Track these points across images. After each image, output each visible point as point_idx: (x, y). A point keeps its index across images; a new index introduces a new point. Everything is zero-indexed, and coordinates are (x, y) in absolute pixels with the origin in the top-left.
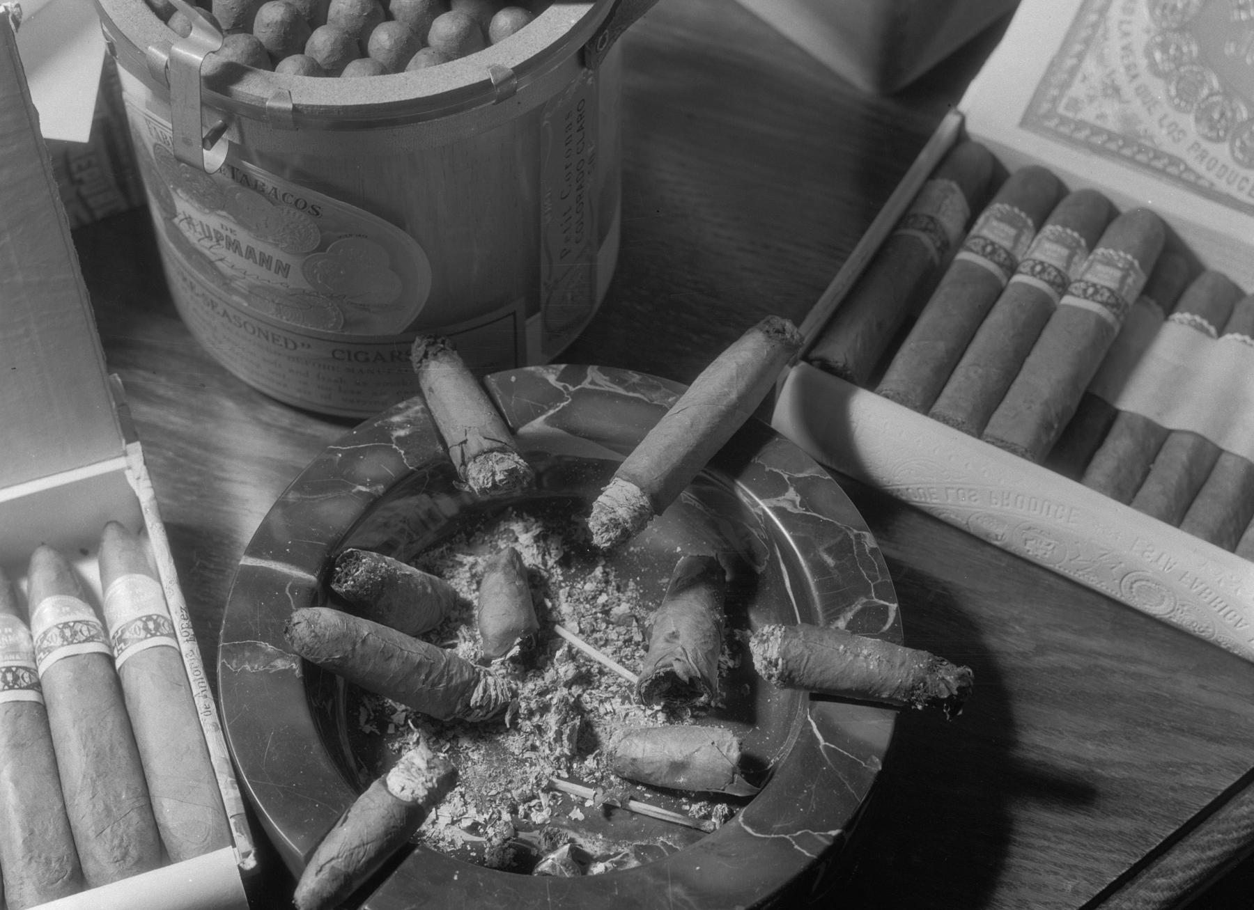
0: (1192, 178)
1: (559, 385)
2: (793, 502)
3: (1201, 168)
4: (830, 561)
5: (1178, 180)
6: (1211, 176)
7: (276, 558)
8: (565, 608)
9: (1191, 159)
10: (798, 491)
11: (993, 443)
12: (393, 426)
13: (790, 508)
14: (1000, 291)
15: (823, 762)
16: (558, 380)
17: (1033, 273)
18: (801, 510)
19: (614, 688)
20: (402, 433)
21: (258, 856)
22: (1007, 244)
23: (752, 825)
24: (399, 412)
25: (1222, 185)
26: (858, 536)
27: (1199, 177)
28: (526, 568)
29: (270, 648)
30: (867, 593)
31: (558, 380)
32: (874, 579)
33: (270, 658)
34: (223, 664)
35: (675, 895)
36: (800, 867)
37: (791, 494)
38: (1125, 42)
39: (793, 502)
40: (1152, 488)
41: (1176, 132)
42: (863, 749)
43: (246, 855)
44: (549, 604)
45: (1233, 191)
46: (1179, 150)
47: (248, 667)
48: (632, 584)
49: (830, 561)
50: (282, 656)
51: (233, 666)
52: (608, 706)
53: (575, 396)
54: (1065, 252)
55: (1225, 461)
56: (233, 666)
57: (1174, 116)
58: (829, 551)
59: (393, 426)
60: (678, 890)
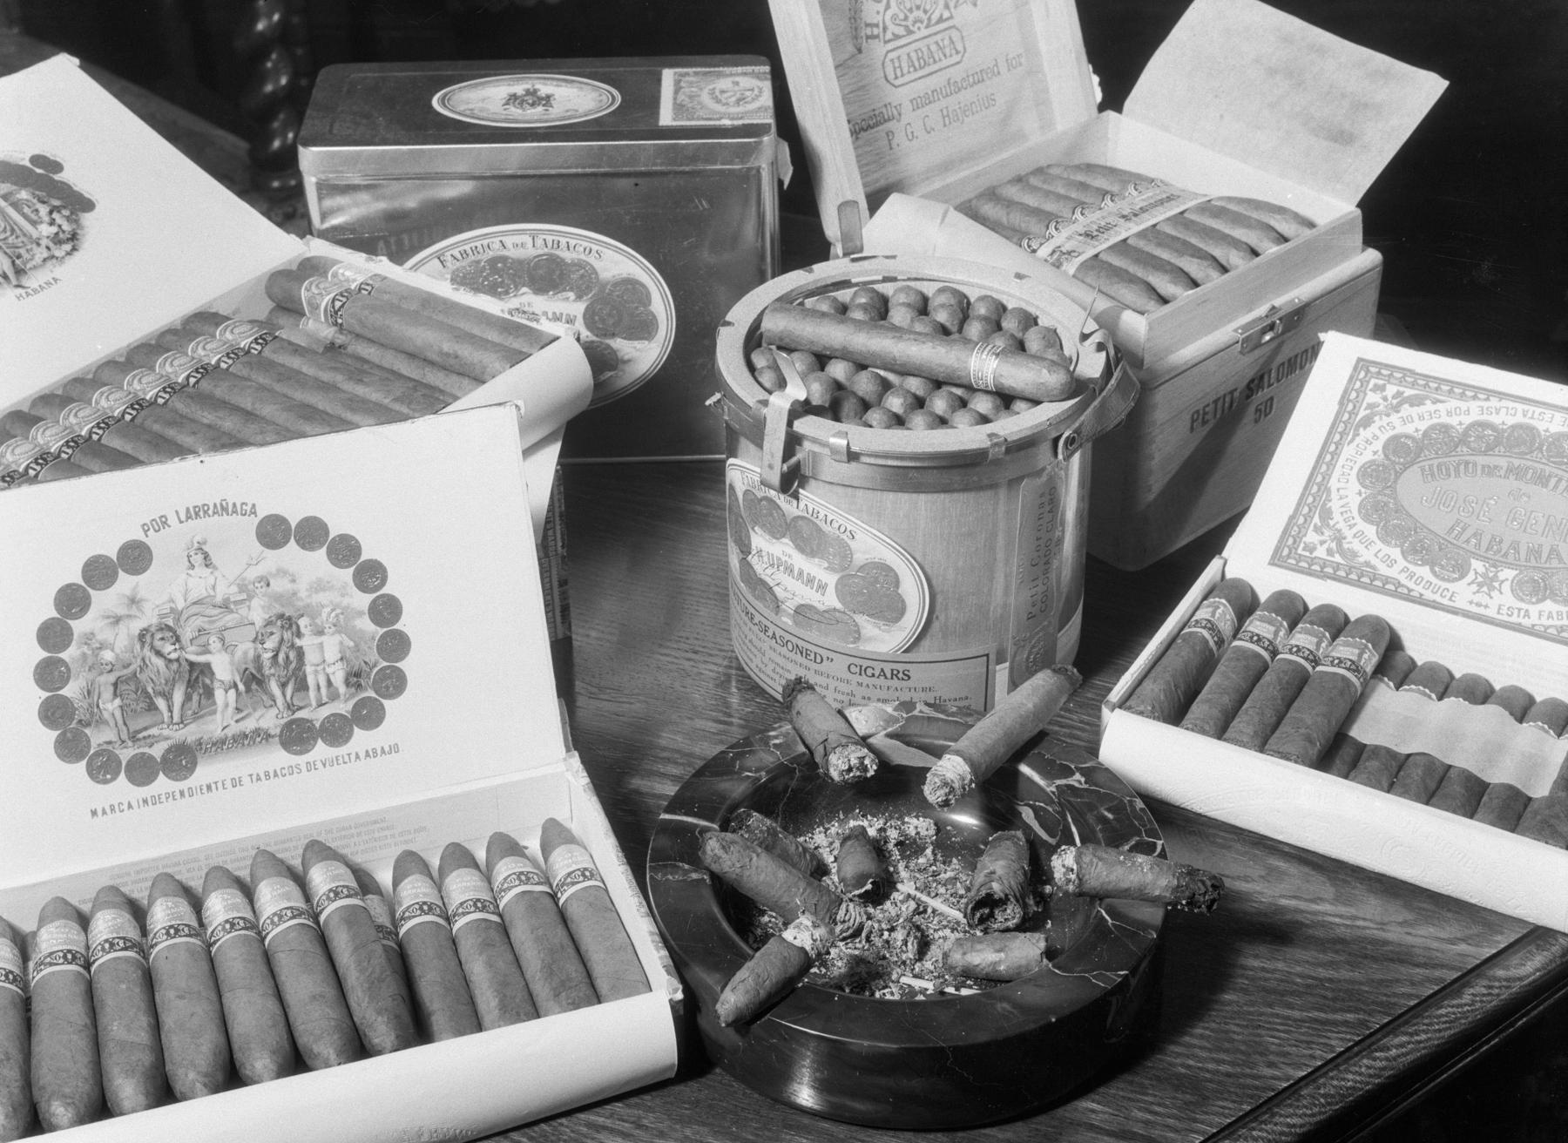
0: (1406, 591)
1: (895, 714)
2: (1080, 782)
3: (1411, 585)
4: (1110, 816)
5: (1395, 594)
6: (1419, 589)
7: (686, 814)
8: (904, 874)
9: (1403, 578)
10: (1082, 775)
11: (1192, 730)
12: (770, 738)
13: (1077, 785)
14: (1266, 667)
15: (1112, 932)
16: (895, 710)
17: (1291, 652)
18: (1086, 786)
19: (945, 923)
20: (777, 741)
21: (684, 991)
22: (1270, 636)
23: (1059, 968)
24: (774, 729)
25: (1428, 595)
26: (1130, 802)
27: (1410, 590)
28: (1118, 317)
29: (686, 867)
30: (1139, 833)
31: (895, 710)
32: (1144, 826)
33: (686, 872)
34: (651, 877)
35: (1004, 1009)
36: (1097, 994)
37: (1078, 776)
38: (1342, 502)
39: (1080, 782)
40: (1198, 709)
41: (1391, 563)
42: (1145, 926)
43: (675, 991)
44: (892, 869)
45: (1437, 598)
46: (1392, 572)
47: (670, 877)
48: (955, 861)
49: (1110, 816)
50: (696, 871)
51: (659, 876)
52: (941, 933)
53: (908, 719)
54: (1315, 640)
55: (1452, 773)
56: (659, 876)
57: (1386, 550)
58: (1109, 810)
59: (770, 738)
60: (1005, 1005)
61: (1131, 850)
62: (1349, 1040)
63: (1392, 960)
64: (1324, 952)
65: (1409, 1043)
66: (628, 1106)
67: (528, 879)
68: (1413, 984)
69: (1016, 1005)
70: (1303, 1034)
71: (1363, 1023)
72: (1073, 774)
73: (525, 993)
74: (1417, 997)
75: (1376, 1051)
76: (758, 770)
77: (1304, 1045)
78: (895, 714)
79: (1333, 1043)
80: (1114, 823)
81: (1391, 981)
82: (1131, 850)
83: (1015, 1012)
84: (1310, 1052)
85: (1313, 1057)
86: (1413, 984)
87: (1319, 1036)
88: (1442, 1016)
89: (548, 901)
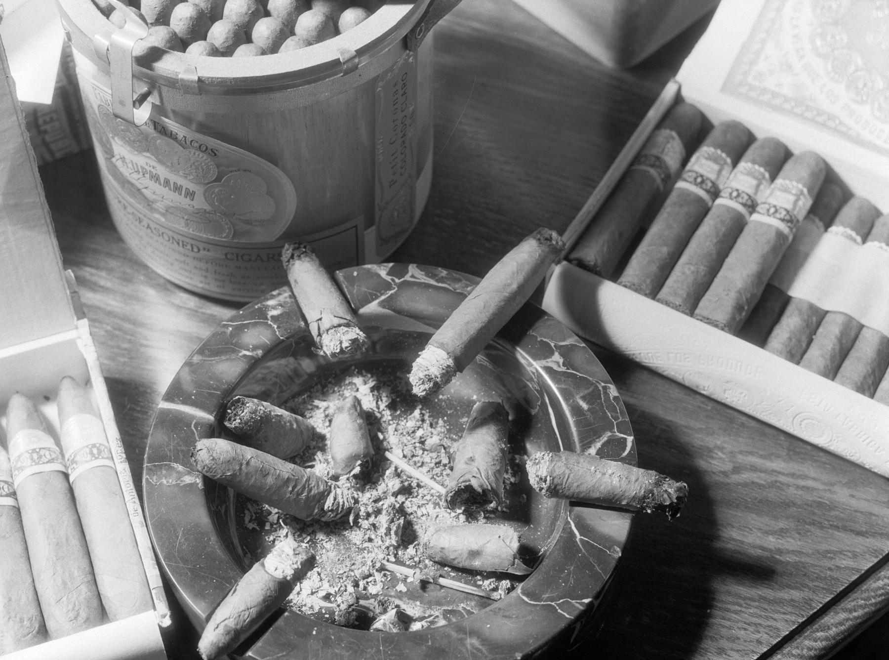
1: (389, 278)
2: (558, 363)
10: (561, 355)
15: (579, 551)
16: (388, 274)
18: (563, 369)
19: (428, 497)
29: (180, 468)
30: (611, 429)
31: (388, 274)
33: (180, 475)
34: (147, 479)
35: (472, 645)
36: (562, 625)
37: (557, 357)
39: (558, 363)
42: (608, 541)
43: (164, 616)
47: (164, 481)
48: (441, 422)
50: (189, 473)
58: (584, 398)
61: (601, 453)
62: (794, 622)
63: (837, 528)
64: (775, 518)
65: (847, 620)
66: (243, 387)
67: (40, 457)
68: (855, 556)
69: (485, 641)
70: (752, 615)
71: (808, 602)
72: (552, 354)
73: (31, 594)
74: (858, 570)
75: (818, 631)
76: (255, 348)
77: (752, 629)
78: (389, 278)
79: (779, 625)
80: (589, 415)
81: (835, 553)
82: (601, 453)
83: (484, 649)
84: (757, 636)
85: (759, 642)
86: (855, 556)
87: (767, 618)
88: (880, 588)
89: (61, 478)
